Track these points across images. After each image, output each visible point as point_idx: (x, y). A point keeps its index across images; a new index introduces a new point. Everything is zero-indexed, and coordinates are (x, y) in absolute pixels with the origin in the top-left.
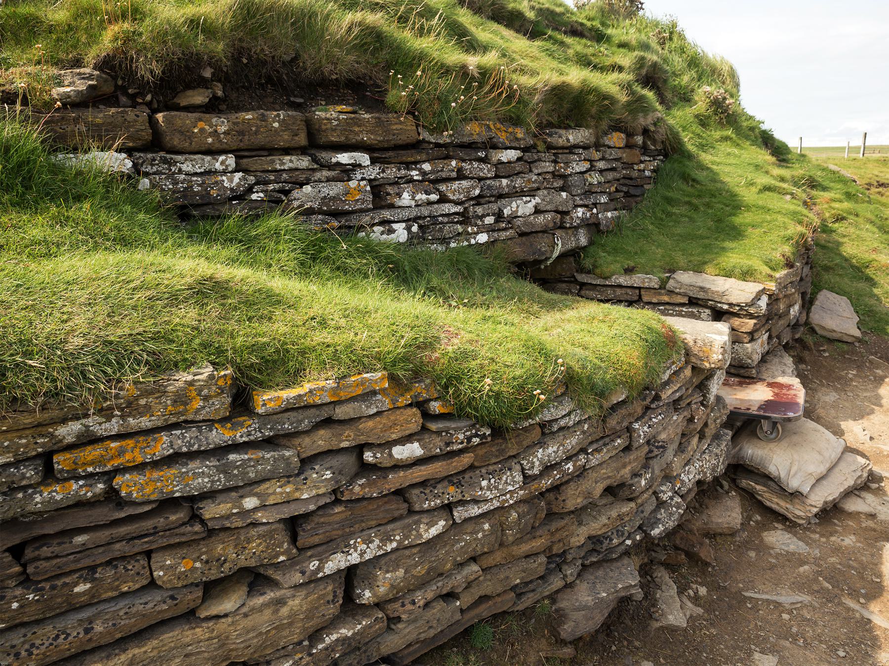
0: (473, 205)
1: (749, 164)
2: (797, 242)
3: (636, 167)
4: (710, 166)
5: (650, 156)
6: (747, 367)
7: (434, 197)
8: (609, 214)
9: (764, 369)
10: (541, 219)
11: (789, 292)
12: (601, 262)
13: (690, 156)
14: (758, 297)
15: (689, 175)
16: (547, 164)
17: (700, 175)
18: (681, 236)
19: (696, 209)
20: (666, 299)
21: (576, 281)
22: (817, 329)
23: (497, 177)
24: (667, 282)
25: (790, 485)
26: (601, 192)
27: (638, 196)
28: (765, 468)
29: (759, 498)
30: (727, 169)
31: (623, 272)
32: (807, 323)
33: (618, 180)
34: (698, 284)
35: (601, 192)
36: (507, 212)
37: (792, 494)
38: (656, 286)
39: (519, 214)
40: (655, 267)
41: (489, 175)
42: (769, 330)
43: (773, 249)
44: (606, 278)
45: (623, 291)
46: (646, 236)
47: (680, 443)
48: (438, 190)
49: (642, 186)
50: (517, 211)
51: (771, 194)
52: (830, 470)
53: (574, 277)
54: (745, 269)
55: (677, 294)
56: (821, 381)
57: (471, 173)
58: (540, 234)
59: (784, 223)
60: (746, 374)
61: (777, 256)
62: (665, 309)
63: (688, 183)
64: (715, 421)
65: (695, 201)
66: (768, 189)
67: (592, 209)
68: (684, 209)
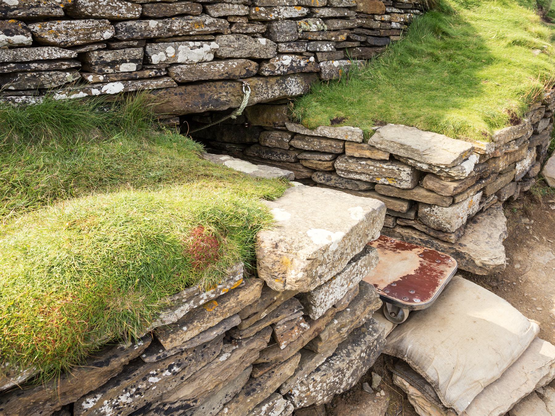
0: (99, 50)
1: (509, 21)
2: (529, 97)
3: (377, 18)
4: (468, 21)
5: (400, 9)
6: (444, 231)
7: (26, 39)
8: (336, 63)
9: (471, 230)
10: (220, 66)
11: (511, 150)
12: (309, 111)
13: (449, 12)
14: (464, 157)
15: (439, 28)
16: (236, 6)
17: (454, 30)
18: (410, 87)
19: (437, 60)
20: (367, 154)
21: (286, 131)
22: (549, 181)
23: (143, 17)
24: (371, 135)
25: (447, 396)
26: (323, 40)
27: (379, 47)
28: (422, 368)
29: (412, 402)
30: (483, 24)
31: (329, 122)
32: (540, 175)
33: (351, 29)
34: (400, 141)
35: (323, 40)
36: (155, 59)
37: (446, 409)
38: (359, 140)
39: (179, 61)
40: (366, 118)
41: (129, 16)
42: (483, 189)
43: (499, 104)
44: (312, 129)
45: (329, 143)
46: (374, 87)
47: (251, 377)
48: (29, 30)
49: (388, 37)
50: (175, 57)
51: (519, 48)
52: (504, 375)
53: (285, 126)
54: (458, 125)
55: (378, 149)
56: (541, 237)
57: (94, 11)
58: (220, 83)
59: (520, 76)
60: (444, 239)
61: (502, 112)
62: (367, 164)
63: (438, 35)
64: (339, 330)
65: (438, 53)
66: (517, 43)
67: (309, 57)
68: (425, 61)
